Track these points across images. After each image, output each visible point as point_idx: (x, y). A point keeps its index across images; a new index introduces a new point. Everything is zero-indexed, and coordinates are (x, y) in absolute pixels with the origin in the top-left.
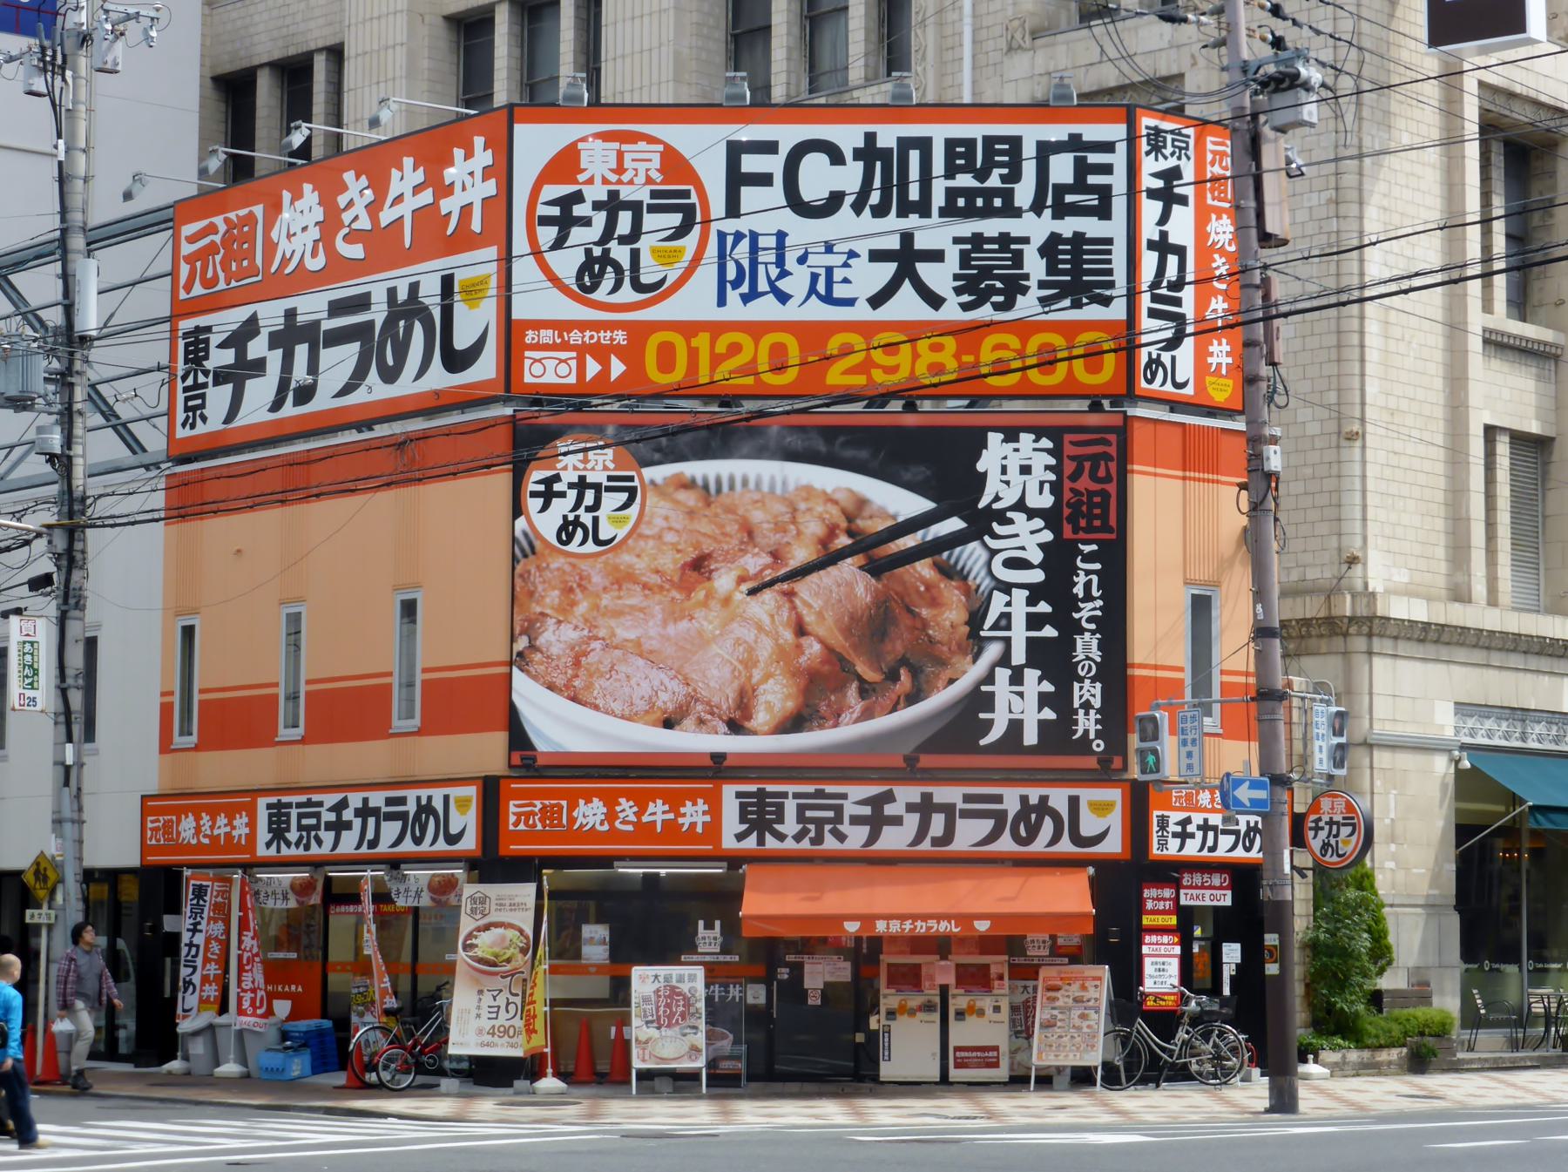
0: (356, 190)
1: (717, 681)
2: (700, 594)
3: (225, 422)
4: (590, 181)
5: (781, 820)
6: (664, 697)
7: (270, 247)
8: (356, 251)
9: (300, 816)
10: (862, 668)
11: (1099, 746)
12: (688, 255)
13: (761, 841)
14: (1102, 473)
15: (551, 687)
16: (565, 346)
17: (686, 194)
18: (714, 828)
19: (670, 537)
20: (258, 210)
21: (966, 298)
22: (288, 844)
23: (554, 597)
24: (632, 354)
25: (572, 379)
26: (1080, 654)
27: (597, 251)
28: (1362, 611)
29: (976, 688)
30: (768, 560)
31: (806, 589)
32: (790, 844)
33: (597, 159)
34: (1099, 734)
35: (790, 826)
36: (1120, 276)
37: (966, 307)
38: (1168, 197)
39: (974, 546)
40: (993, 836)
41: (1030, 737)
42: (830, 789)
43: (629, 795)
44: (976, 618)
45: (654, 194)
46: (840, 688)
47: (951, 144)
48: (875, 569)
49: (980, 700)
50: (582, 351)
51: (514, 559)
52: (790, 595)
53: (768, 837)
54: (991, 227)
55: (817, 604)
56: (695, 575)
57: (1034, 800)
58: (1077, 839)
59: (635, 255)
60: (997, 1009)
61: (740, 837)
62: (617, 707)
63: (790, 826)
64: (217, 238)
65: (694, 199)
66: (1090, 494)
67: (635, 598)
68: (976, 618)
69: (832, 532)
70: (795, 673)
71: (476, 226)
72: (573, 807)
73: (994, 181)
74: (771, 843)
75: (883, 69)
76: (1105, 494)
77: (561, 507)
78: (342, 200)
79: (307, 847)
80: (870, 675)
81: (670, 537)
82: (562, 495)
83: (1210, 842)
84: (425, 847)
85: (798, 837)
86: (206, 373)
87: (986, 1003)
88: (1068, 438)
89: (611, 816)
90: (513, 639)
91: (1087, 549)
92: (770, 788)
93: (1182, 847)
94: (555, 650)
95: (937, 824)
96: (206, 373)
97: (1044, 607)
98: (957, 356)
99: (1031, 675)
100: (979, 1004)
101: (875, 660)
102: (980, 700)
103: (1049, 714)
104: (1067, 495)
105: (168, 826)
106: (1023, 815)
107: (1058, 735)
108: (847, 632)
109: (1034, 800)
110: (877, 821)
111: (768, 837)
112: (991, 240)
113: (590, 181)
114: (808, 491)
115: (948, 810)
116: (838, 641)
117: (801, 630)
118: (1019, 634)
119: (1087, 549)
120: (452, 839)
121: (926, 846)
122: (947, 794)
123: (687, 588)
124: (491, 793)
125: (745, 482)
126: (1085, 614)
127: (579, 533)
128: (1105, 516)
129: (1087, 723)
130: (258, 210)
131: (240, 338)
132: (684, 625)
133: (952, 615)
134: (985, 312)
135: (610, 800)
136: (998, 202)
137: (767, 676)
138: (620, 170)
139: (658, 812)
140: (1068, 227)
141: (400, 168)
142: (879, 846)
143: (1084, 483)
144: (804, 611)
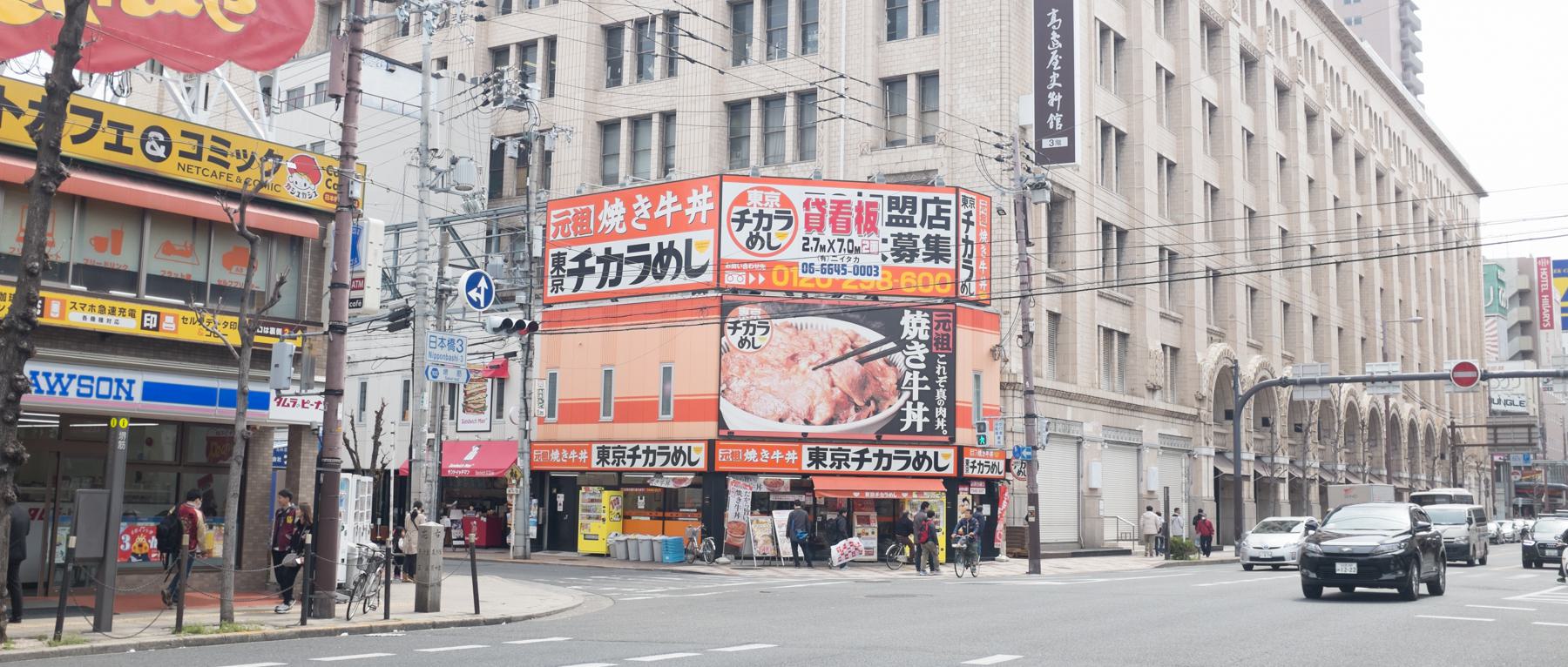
0: (642, 201)
1: (801, 406)
2: (793, 369)
3: (574, 291)
4: (752, 206)
5: (825, 459)
6: (779, 410)
7: (598, 223)
8: (643, 227)
9: (614, 452)
10: (856, 401)
11: (945, 432)
12: (790, 236)
13: (817, 467)
14: (947, 327)
15: (735, 405)
16: (741, 270)
17: (789, 212)
18: (799, 462)
19: (782, 347)
20: (592, 207)
21: (896, 258)
22: (608, 463)
23: (736, 369)
24: (767, 273)
25: (744, 283)
26: (938, 397)
27: (754, 233)
28: (1012, 380)
29: (899, 410)
30: (821, 357)
31: (834, 367)
32: (828, 469)
33: (755, 198)
34: (945, 428)
35: (828, 462)
36: (953, 252)
37: (895, 261)
38: (969, 223)
39: (900, 353)
40: (906, 467)
41: (920, 429)
42: (844, 447)
43: (766, 448)
44: (900, 383)
45: (777, 212)
46: (848, 408)
47: (890, 198)
48: (862, 362)
49: (901, 414)
50: (748, 271)
51: (721, 353)
52: (829, 370)
53: (820, 466)
54: (905, 231)
55: (839, 375)
56: (791, 362)
57: (921, 453)
58: (937, 468)
59: (769, 235)
60: (873, 533)
61: (809, 465)
62: (761, 413)
63: (828, 462)
64: (570, 217)
65: (792, 214)
66: (943, 335)
67: (768, 370)
68: (900, 383)
69: (845, 346)
70: (831, 402)
71: (703, 220)
72: (744, 452)
73: (906, 213)
74: (821, 468)
75: (798, 158)
76: (948, 336)
77: (740, 333)
78: (635, 206)
79: (618, 465)
80: (860, 403)
81: (782, 347)
82: (740, 328)
83: (651, 460)
84: (679, 466)
85: (832, 466)
86: (564, 271)
87: (869, 530)
88: (934, 313)
89: (759, 456)
90: (720, 385)
91: (941, 356)
92: (821, 446)
93: (633, 464)
94: (737, 390)
95: (885, 462)
96: (564, 271)
97: (925, 378)
98: (892, 280)
99: (920, 404)
100: (866, 531)
101: (861, 396)
102: (901, 414)
103: (927, 420)
104: (934, 335)
105: (545, 455)
106: (917, 459)
107: (930, 428)
108: (851, 386)
109: (921, 453)
110: (862, 460)
111: (820, 466)
112: (905, 236)
113: (752, 206)
114: (836, 331)
115: (889, 456)
116: (847, 389)
117: (833, 385)
118: (916, 389)
119: (941, 356)
120: (692, 464)
121: (880, 470)
122: (888, 450)
123: (788, 366)
124: (711, 446)
125: (817, 327)
126: (940, 381)
127: (747, 344)
128: (948, 344)
129: (941, 424)
130: (592, 207)
131: (582, 258)
132: (787, 381)
133: (890, 381)
134: (903, 264)
135: (759, 450)
136: (907, 221)
137: (820, 402)
138: (764, 202)
139: (777, 455)
140: (934, 232)
141: (665, 195)
142: (863, 470)
143: (940, 331)
144: (834, 377)
